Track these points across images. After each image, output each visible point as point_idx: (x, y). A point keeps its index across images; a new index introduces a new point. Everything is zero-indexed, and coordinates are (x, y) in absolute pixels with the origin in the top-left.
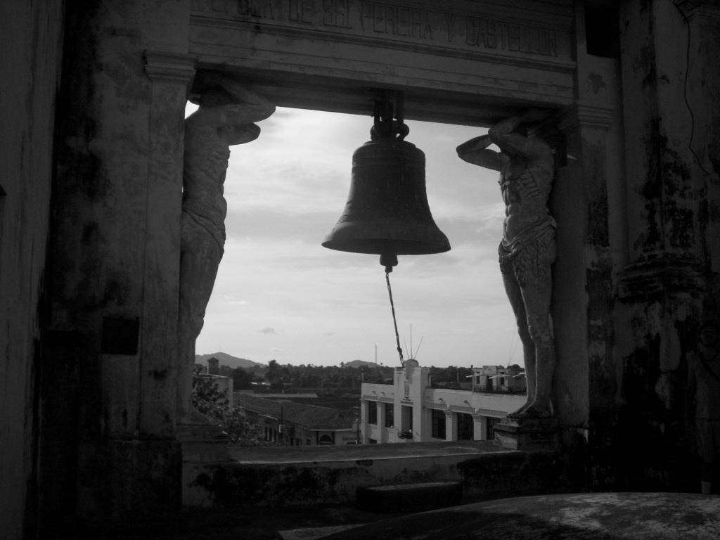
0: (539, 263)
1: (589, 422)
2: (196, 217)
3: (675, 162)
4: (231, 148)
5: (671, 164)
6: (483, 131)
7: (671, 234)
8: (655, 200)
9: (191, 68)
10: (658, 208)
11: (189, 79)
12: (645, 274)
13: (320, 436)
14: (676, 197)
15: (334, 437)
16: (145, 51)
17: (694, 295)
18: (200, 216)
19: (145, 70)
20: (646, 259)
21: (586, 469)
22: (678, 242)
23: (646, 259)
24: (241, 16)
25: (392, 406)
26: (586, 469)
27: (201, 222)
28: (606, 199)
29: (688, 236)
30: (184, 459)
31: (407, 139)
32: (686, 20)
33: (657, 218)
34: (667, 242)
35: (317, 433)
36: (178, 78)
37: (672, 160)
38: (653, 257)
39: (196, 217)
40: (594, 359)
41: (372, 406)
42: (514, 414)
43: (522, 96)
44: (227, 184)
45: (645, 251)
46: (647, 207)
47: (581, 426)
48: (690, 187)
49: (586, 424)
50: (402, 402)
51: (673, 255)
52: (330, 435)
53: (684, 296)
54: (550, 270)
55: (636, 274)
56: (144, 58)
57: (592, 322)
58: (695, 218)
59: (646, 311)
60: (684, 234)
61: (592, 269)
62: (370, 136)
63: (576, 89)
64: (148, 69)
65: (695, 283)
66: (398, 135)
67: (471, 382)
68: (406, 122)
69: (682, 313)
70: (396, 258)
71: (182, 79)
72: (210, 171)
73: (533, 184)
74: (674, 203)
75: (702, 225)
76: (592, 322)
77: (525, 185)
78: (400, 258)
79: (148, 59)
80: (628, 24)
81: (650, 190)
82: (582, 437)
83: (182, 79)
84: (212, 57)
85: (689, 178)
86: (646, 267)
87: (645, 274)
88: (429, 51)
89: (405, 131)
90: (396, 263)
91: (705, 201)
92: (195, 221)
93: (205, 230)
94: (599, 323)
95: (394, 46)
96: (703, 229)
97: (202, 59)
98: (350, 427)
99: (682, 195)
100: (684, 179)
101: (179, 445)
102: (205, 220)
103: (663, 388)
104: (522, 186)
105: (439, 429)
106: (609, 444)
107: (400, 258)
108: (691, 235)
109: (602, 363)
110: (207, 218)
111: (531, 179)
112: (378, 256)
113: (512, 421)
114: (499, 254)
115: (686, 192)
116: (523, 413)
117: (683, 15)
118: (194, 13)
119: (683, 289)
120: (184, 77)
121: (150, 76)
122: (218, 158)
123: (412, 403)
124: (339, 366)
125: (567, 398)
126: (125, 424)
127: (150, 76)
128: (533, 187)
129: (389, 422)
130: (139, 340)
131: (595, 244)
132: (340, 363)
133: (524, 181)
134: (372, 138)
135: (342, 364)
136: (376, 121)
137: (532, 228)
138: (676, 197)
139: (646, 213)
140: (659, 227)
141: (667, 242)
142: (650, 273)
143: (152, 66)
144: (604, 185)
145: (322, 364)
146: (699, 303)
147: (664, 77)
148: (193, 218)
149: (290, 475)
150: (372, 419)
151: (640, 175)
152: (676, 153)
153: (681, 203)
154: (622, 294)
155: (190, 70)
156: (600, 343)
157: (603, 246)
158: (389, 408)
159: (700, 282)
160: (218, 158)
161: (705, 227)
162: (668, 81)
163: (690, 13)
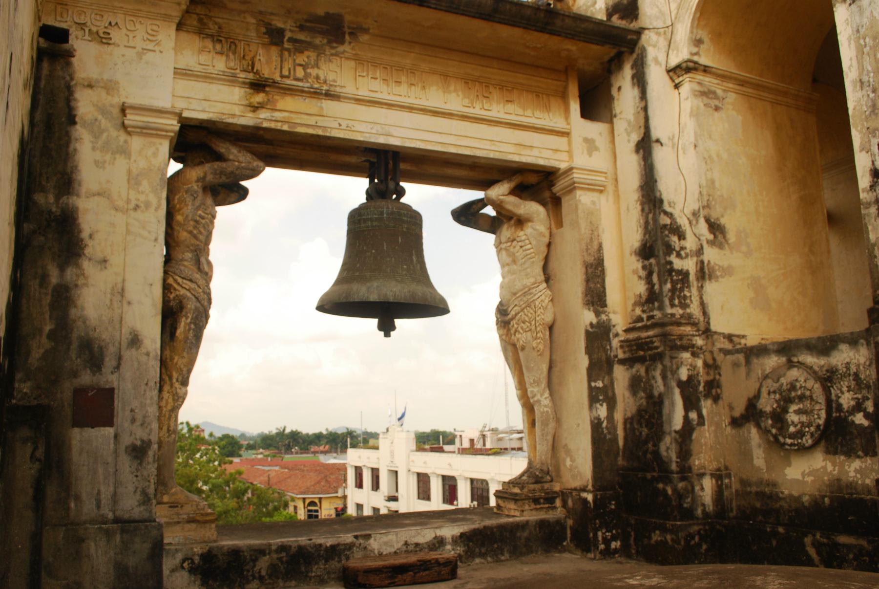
0: (537, 324)
1: (593, 486)
2: (180, 280)
3: (671, 224)
4: (218, 209)
5: (667, 225)
6: (477, 195)
7: (670, 294)
8: (652, 261)
9: (175, 122)
10: (656, 269)
11: (172, 134)
12: (644, 334)
13: (307, 501)
14: (673, 258)
15: (320, 502)
16: (124, 103)
17: (694, 355)
18: (183, 278)
19: (123, 123)
20: (645, 319)
21: (591, 535)
22: (676, 302)
23: (645, 319)
24: (229, 70)
25: (377, 470)
26: (591, 535)
27: (184, 286)
28: (603, 260)
29: (685, 296)
30: (166, 541)
31: (403, 200)
32: (677, 86)
33: (655, 278)
34: (667, 302)
35: (304, 499)
36: (159, 133)
37: (668, 221)
38: (652, 317)
39: (180, 280)
40: (596, 421)
41: (359, 471)
42: (515, 479)
43: (516, 158)
44: (212, 247)
45: (643, 311)
46: (644, 268)
47: (584, 490)
48: (685, 248)
49: (590, 487)
50: (388, 466)
51: (673, 315)
52: (317, 501)
53: (686, 355)
54: (548, 333)
55: (632, 336)
56: (123, 110)
57: (593, 384)
58: (692, 277)
59: (647, 371)
60: (682, 294)
61: (590, 330)
62: (364, 196)
63: (570, 152)
64: (126, 122)
65: (694, 342)
66: (394, 196)
67: (378, 439)
68: (402, 184)
69: (684, 374)
70: (394, 322)
71: (164, 133)
72: (195, 232)
73: (529, 246)
74: (671, 263)
75: (700, 285)
76: (593, 384)
77: (521, 247)
78: (398, 322)
79: (127, 111)
80: (619, 88)
81: (646, 252)
82: (585, 501)
83: (164, 133)
84: (198, 112)
85: (684, 239)
86: (646, 328)
87: (644, 334)
88: (425, 111)
89: (401, 192)
90: (393, 328)
91: (702, 262)
92: (178, 284)
93: (189, 294)
94: (600, 384)
95: (390, 106)
96: (701, 288)
97: (186, 114)
98: (337, 492)
99: (679, 255)
100: (679, 239)
101: (160, 527)
102: (188, 282)
103: (668, 448)
104: (518, 248)
105: (424, 493)
106: (613, 507)
107: (398, 322)
108: (688, 294)
109: (604, 425)
110: (191, 280)
111: (527, 242)
112: (375, 321)
113: (514, 486)
114: (497, 317)
115: (683, 253)
116: (524, 478)
117: (673, 81)
118: (177, 67)
119: (685, 348)
120: (167, 131)
121: (129, 129)
122: (203, 218)
123: (397, 467)
124: (325, 432)
125: (568, 462)
126: (98, 507)
127: (129, 129)
128: (529, 249)
129: (376, 486)
130: (311, 131)
131: (593, 305)
132: (325, 428)
133: (520, 244)
134: (367, 199)
135: (327, 430)
136: (371, 182)
137: (529, 290)
138: (673, 258)
139: (643, 273)
140: (657, 287)
141: (667, 302)
142: (651, 333)
143: (132, 118)
144: (600, 247)
145: (280, 426)
146: (699, 363)
147: (658, 141)
148: (175, 281)
149: (284, 554)
150: (359, 485)
151: (634, 237)
152: (671, 214)
153: (678, 264)
154: (621, 355)
155: (174, 125)
156: (601, 405)
157: (602, 307)
158: (375, 473)
159: (699, 341)
160: (203, 218)
161: (702, 287)
162: (662, 145)
163: (681, 79)
